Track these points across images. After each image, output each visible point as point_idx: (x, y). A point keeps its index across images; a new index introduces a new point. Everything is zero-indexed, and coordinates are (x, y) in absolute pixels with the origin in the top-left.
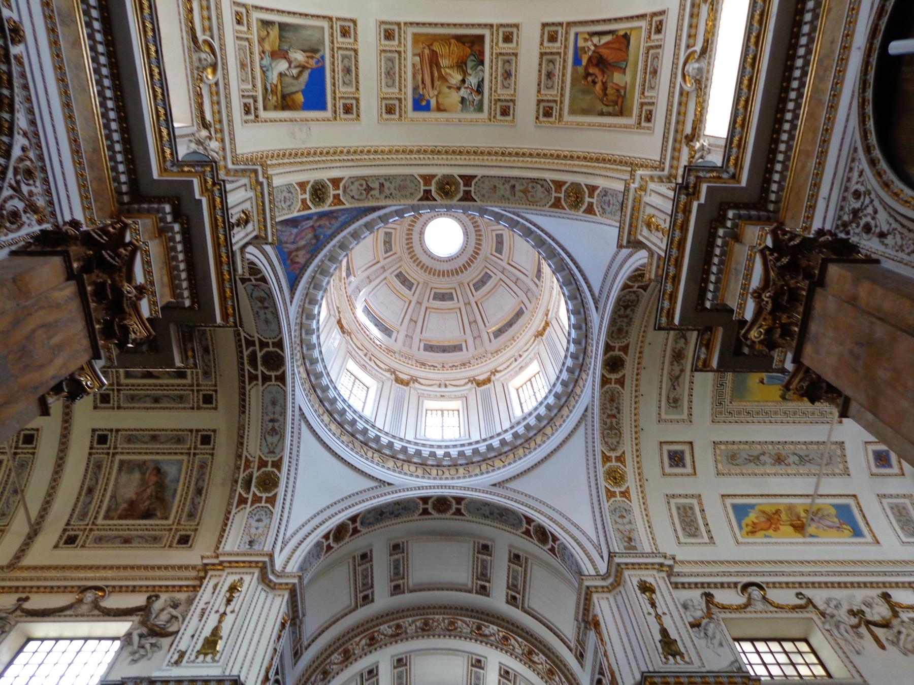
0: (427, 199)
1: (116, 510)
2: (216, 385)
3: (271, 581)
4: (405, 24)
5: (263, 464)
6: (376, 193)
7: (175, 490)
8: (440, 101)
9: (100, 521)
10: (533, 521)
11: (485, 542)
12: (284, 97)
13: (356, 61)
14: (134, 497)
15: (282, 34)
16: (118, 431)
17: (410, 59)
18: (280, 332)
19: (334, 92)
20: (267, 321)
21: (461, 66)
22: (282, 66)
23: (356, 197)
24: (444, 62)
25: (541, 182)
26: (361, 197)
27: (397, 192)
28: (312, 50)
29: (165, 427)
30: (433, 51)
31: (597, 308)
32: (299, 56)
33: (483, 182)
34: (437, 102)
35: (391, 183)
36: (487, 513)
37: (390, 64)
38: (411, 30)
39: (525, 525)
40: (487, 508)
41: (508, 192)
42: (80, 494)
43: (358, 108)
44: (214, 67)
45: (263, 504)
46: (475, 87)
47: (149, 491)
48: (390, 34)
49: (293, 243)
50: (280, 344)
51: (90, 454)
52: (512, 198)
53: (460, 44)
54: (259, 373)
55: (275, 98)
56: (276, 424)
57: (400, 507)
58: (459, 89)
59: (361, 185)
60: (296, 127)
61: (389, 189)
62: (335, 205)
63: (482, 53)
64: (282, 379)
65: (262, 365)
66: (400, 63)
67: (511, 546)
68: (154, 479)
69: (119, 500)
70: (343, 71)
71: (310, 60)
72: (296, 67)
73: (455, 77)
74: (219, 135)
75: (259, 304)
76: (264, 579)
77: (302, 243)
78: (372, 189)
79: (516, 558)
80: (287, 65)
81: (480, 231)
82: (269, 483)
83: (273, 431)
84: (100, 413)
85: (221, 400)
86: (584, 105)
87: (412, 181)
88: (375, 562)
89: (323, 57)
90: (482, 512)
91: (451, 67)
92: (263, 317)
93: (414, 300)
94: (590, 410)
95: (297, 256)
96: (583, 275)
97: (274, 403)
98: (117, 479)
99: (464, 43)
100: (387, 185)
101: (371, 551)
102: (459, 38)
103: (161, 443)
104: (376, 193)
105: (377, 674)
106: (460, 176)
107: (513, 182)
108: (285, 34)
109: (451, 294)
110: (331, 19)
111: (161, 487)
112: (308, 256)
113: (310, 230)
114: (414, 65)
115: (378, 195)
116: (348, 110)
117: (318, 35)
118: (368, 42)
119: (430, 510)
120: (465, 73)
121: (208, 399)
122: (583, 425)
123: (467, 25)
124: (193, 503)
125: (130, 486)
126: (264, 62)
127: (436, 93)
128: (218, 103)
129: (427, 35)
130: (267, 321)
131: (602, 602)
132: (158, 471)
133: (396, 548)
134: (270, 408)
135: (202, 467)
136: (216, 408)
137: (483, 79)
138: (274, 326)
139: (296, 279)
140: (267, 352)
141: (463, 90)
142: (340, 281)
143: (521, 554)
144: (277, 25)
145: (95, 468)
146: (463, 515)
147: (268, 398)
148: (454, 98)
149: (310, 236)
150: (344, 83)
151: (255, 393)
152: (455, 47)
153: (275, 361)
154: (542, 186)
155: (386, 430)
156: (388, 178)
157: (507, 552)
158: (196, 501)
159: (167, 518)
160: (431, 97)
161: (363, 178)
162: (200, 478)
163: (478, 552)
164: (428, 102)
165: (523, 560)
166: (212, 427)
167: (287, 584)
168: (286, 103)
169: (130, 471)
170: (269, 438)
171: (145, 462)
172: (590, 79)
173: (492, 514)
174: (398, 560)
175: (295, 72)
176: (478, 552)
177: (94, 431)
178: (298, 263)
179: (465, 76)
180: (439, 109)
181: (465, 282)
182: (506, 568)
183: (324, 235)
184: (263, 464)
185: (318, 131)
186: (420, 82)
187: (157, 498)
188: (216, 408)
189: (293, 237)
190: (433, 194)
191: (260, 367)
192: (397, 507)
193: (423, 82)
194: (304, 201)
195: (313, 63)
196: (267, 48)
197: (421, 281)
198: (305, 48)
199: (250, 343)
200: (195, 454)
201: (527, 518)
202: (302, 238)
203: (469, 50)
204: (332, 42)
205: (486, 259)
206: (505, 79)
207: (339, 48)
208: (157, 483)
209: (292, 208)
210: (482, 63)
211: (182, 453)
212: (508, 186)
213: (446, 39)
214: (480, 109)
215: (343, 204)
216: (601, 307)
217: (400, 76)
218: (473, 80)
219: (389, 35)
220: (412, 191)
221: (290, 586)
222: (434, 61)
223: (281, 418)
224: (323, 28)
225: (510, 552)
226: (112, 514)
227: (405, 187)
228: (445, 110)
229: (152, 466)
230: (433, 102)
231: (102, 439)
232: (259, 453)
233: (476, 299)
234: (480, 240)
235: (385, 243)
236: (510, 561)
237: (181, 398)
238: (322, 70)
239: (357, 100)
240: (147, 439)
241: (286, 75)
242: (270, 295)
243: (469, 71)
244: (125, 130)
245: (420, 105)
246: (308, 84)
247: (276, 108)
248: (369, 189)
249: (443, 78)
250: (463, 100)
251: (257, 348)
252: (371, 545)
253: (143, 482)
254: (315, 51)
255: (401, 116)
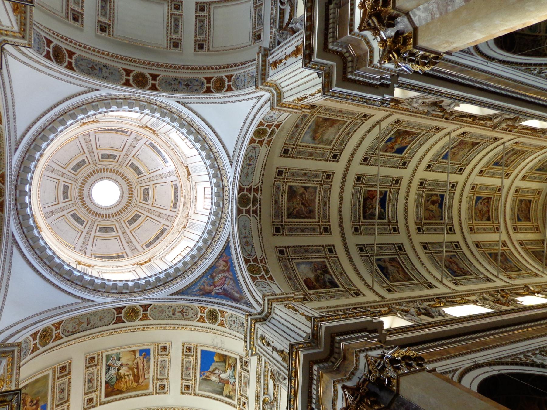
0: (145, 306)
1: (340, 124)
2: (275, 181)
3: (275, 90)
4: (153, 394)
5: (261, 143)
6: (178, 310)
7: (308, 129)
8: (133, 356)
9: (349, 121)
10: (66, 67)
11: (103, 34)
12: (225, 361)
13: (182, 374)
14: (330, 128)
15: (221, 390)
16: (327, 160)
17: (151, 376)
18: (238, 220)
19: (196, 359)
20: (245, 227)
21: (120, 377)
22: (223, 376)
23: (190, 309)
24: (131, 377)
25: (70, 333)
26: (187, 308)
27: (164, 309)
28: (206, 380)
29: (305, 160)
30: (137, 382)
31: (13, 236)
32: (214, 378)
33: (108, 321)
34: (135, 355)
35: (168, 315)
36: (104, 69)
37: (163, 372)
38: (150, 391)
39: (73, 61)
40: (105, 75)
41: (91, 320)
42: (353, 133)
43: (183, 349)
44: (264, 402)
45: (266, 124)
46: (112, 368)
47: (322, 130)
48: (162, 388)
49: (227, 277)
50: (239, 212)
51: (342, 150)
52: (89, 316)
53: (120, 389)
54: (252, 193)
55: (230, 362)
56: (248, 162)
57: (173, 86)
58: (121, 365)
59: (186, 315)
60: (220, 345)
61: (169, 311)
62: (204, 307)
63: (106, 388)
64: (241, 189)
65: (250, 198)
66: (157, 373)
67: (82, 30)
68: (317, 135)
69: (337, 128)
70: (190, 369)
71: (208, 375)
72: (217, 374)
73: (123, 371)
74: (267, 369)
75: (248, 240)
76: (280, 94)
77: (221, 275)
78: (180, 312)
79: (77, 17)
80: (221, 375)
81: (80, 199)
82: (260, 132)
83: (250, 159)
84: (333, 169)
85: (274, 172)
86: (38, 385)
87: (155, 316)
88: (193, 39)
89: (201, 376)
90: (108, 71)
91: (126, 376)
92: (247, 231)
93: (147, 214)
94: (13, 150)
95: (224, 266)
96: (30, 264)
97: (247, 175)
98: (335, 137)
99: (118, 390)
100: (171, 314)
101: (195, 50)
102: (121, 392)
103: (308, 152)
104: (178, 310)
105: (69, 373)
106: (124, 322)
107: (89, 326)
108: (221, 390)
109: (102, 158)
110: (195, 394)
111: (315, 131)
112: (217, 264)
113: (217, 284)
114: (149, 373)
115: (177, 308)
116: (189, 349)
117: (203, 387)
118: (175, 382)
119: (150, 78)
120: (118, 374)
121: (280, 173)
122: (18, 136)
123: (116, 400)
124: (302, 121)
125: (330, 133)
126: (233, 381)
127: (136, 360)
128: (264, 384)
129: (140, 390)
130: (245, 227)
131: (9, 25)
132: (314, 139)
133: (176, 45)
134: (250, 171)
135: (314, 229)
136: (277, 168)
137: (106, 373)
138: (242, 224)
139: (225, 250)
140: (246, 206)
141: (119, 365)
142: (185, 195)
143: (72, 22)
144: (224, 395)
145: (343, 144)
146: (124, 69)
147: (250, 178)
148: (124, 360)
149: (216, 279)
150: (190, 363)
151: (256, 181)
152: (123, 386)
153: (243, 201)
154: (68, 332)
155: (200, 234)
156: (170, 318)
157: (85, 23)
158: (300, 122)
159: (318, 117)
160: (138, 358)
161: (185, 319)
162: (294, 133)
163: (109, 25)
164: (141, 355)
165: (70, 16)
166: (281, 158)
167: (266, 86)
168: (224, 358)
169: (327, 140)
170: (254, 155)
171: (319, 143)
172: (35, 402)
173: (101, 69)
174: (176, 32)
175: (217, 372)
176: (109, 25)
177: (337, 161)
178: (223, 261)
179: (117, 373)
180: (134, 351)
181: (91, 165)
182: (85, 8)
183: (207, 278)
184: (261, 143)
185: (206, 337)
186: (145, 365)
187: (319, 126)
188: (277, 168)
189: (227, 282)
190: (141, 309)
191: (251, 197)
192: (176, 87)
193: (144, 365)
194: (223, 316)
195: (207, 374)
196: (231, 387)
197: (124, 167)
198: (210, 382)
199: (255, 212)
200: (294, 145)
201: (72, 69)
202: (221, 279)
203: (115, 387)
204: (195, 383)
205: (76, 181)
206: (91, 378)
207: (191, 380)
208: (316, 133)
209: (230, 316)
210: (107, 382)
211: (300, 146)
212: (92, 323)
213: (129, 390)
214: (108, 357)
215: (198, 307)
216: (10, 238)
217: (157, 367)
218: (113, 371)
219: (162, 387)
220: (155, 310)
221: (265, 84)
222: (136, 377)
223: (245, 166)
224: (199, 390)
225: (82, 24)
226: (343, 123)
227: (159, 312)
228: (130, 351)
229: (316, 141)
230: (138, 355)
231: (335, 156)
232: (261, 148)
233: (85, 155)
234: (80, 193)
235: (148, 195)
236: (82, 14)
237: (293, 175)
238: (201, 370)
239: (183, 354)
240: (325, 199)
241: (222, 371)
242: (243, 248)
243: (115, 376)
244: (311, 379)
245: (146, 353)
246: (211, 365)
247: (230, 357)
248: (182, 312)
249: (131, 369)
250: (119, 359)
251: (251, 209)
252: (195, 55)
253: (323, 134)
254: (204, 379)
255: (158, 346)
